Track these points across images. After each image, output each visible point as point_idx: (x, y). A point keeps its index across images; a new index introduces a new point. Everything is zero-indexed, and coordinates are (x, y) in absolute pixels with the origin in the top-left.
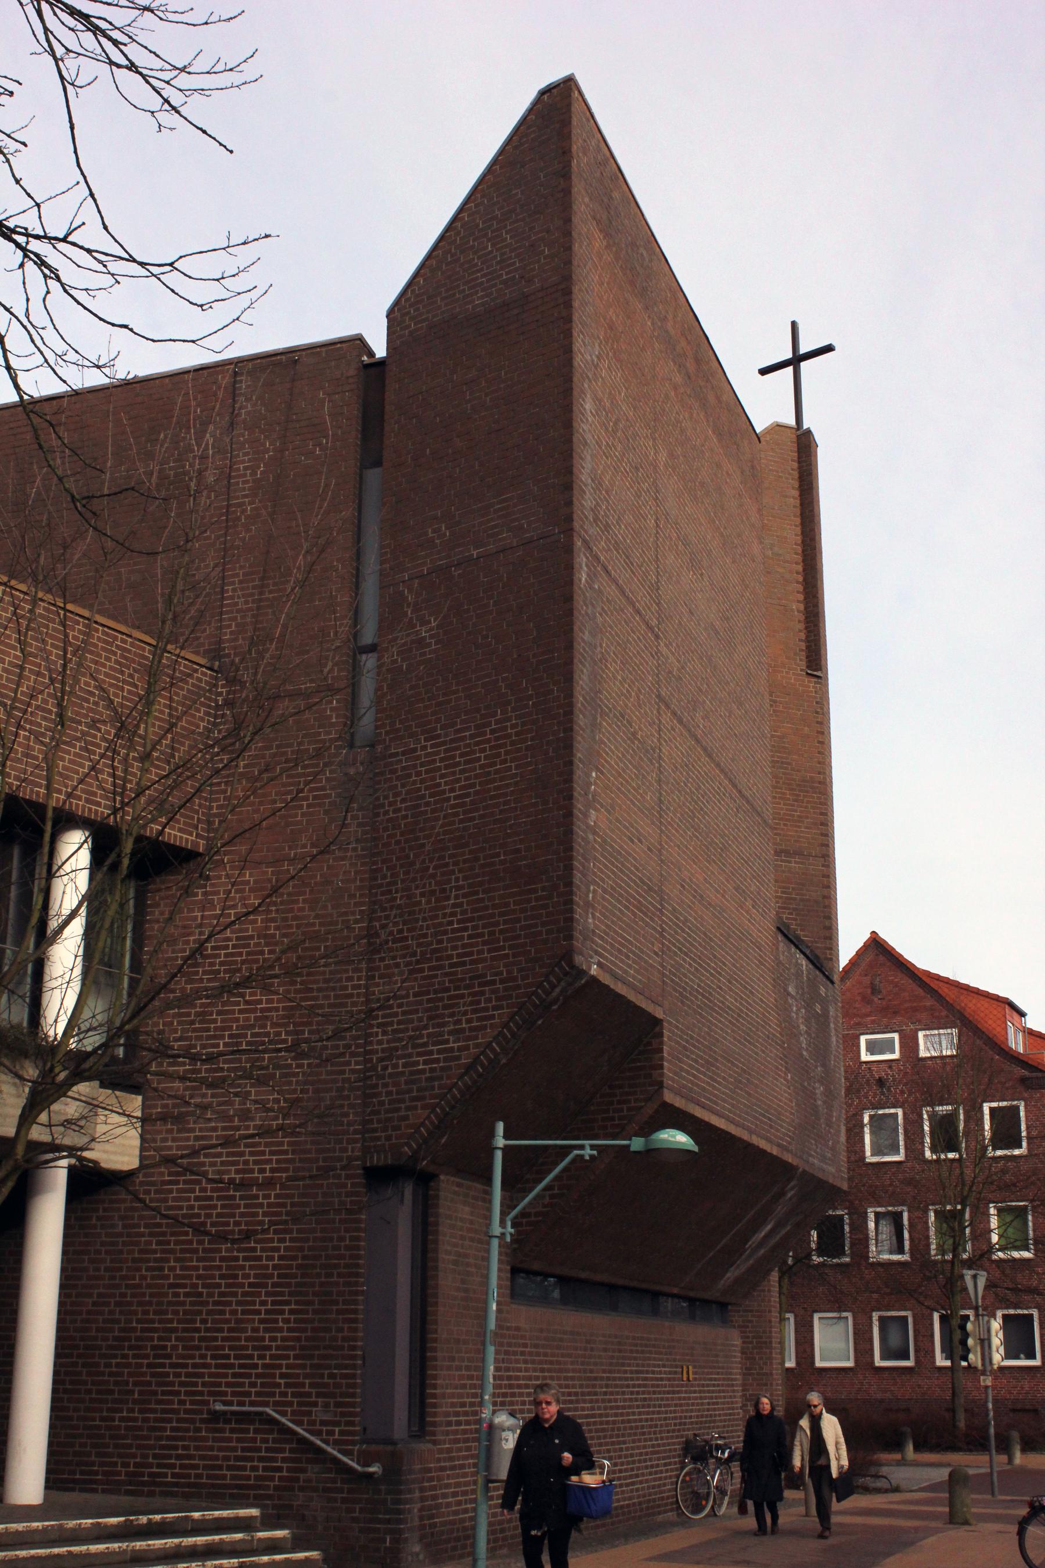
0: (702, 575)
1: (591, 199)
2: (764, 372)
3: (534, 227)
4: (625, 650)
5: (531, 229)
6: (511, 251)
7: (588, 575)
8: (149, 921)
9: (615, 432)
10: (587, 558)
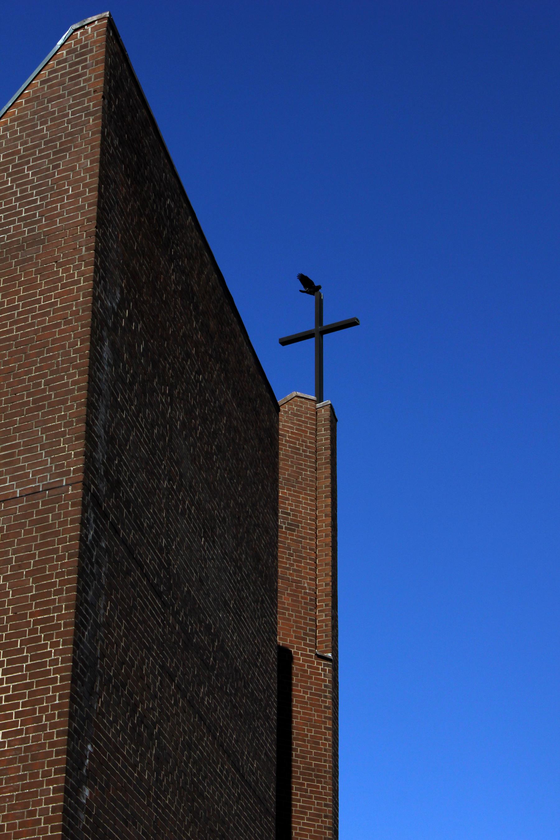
0: (214, 542)
1: (120, 143)
2: (285, 342)
3: (58, 166)
4: (240, 616)
5: (55, 167)
6: (32, 188)
7: (96, 532)
8: (327, 463)
9: (132, 384)
10: (95, 513)
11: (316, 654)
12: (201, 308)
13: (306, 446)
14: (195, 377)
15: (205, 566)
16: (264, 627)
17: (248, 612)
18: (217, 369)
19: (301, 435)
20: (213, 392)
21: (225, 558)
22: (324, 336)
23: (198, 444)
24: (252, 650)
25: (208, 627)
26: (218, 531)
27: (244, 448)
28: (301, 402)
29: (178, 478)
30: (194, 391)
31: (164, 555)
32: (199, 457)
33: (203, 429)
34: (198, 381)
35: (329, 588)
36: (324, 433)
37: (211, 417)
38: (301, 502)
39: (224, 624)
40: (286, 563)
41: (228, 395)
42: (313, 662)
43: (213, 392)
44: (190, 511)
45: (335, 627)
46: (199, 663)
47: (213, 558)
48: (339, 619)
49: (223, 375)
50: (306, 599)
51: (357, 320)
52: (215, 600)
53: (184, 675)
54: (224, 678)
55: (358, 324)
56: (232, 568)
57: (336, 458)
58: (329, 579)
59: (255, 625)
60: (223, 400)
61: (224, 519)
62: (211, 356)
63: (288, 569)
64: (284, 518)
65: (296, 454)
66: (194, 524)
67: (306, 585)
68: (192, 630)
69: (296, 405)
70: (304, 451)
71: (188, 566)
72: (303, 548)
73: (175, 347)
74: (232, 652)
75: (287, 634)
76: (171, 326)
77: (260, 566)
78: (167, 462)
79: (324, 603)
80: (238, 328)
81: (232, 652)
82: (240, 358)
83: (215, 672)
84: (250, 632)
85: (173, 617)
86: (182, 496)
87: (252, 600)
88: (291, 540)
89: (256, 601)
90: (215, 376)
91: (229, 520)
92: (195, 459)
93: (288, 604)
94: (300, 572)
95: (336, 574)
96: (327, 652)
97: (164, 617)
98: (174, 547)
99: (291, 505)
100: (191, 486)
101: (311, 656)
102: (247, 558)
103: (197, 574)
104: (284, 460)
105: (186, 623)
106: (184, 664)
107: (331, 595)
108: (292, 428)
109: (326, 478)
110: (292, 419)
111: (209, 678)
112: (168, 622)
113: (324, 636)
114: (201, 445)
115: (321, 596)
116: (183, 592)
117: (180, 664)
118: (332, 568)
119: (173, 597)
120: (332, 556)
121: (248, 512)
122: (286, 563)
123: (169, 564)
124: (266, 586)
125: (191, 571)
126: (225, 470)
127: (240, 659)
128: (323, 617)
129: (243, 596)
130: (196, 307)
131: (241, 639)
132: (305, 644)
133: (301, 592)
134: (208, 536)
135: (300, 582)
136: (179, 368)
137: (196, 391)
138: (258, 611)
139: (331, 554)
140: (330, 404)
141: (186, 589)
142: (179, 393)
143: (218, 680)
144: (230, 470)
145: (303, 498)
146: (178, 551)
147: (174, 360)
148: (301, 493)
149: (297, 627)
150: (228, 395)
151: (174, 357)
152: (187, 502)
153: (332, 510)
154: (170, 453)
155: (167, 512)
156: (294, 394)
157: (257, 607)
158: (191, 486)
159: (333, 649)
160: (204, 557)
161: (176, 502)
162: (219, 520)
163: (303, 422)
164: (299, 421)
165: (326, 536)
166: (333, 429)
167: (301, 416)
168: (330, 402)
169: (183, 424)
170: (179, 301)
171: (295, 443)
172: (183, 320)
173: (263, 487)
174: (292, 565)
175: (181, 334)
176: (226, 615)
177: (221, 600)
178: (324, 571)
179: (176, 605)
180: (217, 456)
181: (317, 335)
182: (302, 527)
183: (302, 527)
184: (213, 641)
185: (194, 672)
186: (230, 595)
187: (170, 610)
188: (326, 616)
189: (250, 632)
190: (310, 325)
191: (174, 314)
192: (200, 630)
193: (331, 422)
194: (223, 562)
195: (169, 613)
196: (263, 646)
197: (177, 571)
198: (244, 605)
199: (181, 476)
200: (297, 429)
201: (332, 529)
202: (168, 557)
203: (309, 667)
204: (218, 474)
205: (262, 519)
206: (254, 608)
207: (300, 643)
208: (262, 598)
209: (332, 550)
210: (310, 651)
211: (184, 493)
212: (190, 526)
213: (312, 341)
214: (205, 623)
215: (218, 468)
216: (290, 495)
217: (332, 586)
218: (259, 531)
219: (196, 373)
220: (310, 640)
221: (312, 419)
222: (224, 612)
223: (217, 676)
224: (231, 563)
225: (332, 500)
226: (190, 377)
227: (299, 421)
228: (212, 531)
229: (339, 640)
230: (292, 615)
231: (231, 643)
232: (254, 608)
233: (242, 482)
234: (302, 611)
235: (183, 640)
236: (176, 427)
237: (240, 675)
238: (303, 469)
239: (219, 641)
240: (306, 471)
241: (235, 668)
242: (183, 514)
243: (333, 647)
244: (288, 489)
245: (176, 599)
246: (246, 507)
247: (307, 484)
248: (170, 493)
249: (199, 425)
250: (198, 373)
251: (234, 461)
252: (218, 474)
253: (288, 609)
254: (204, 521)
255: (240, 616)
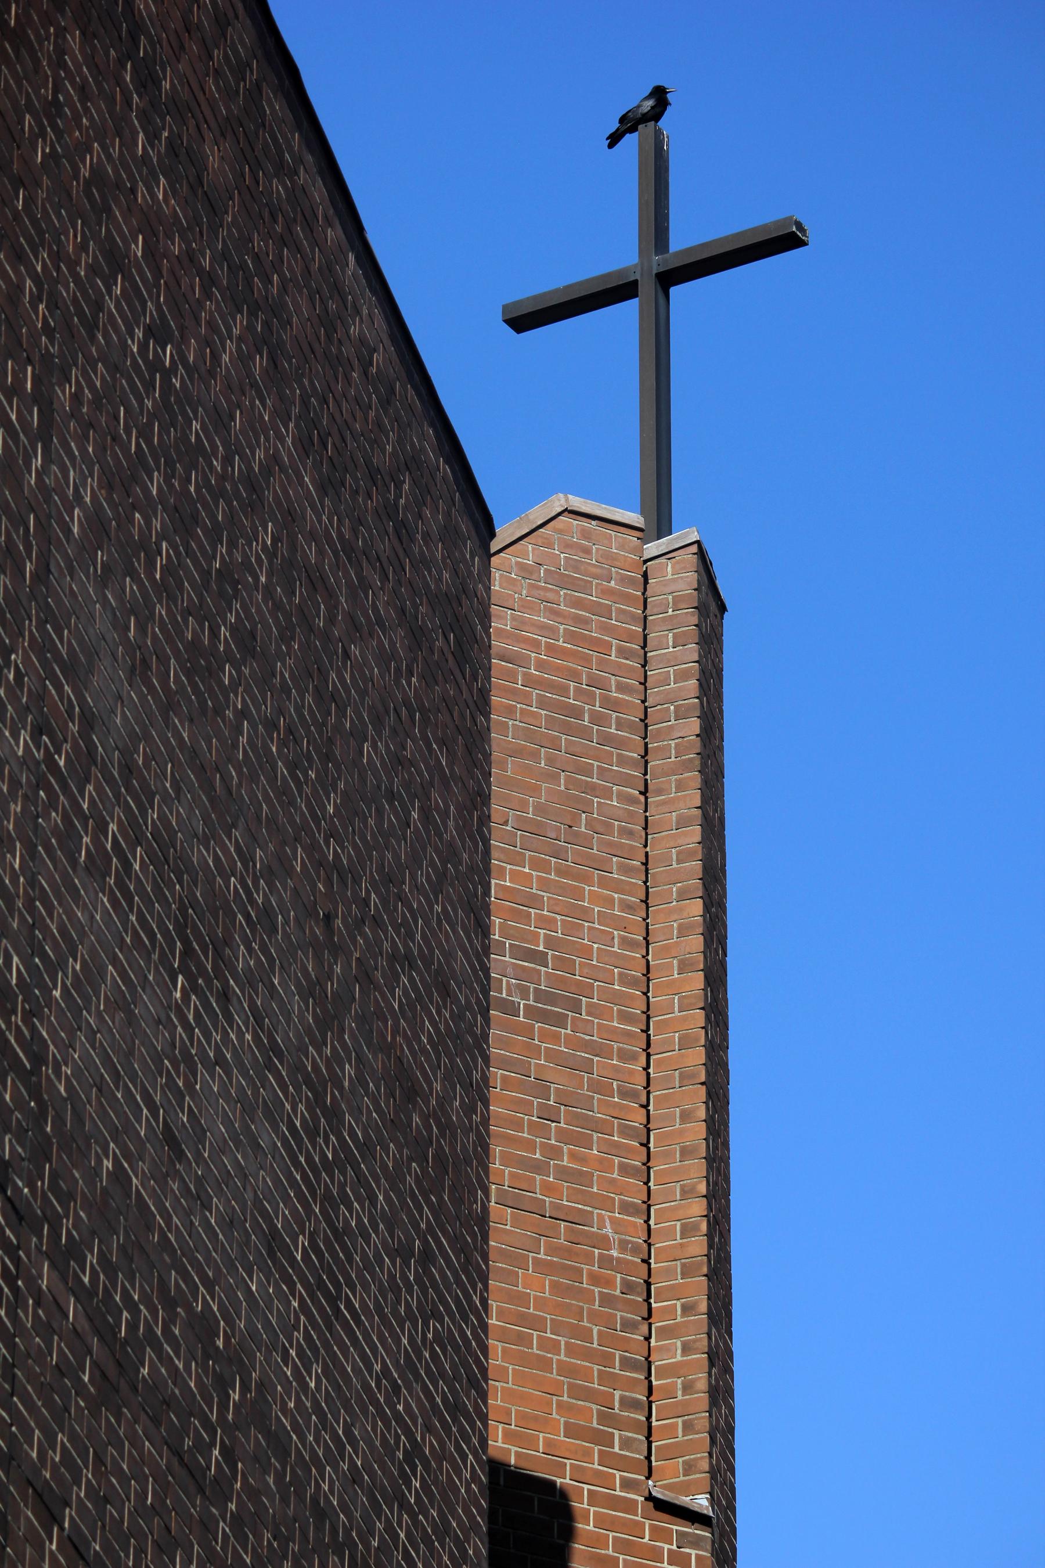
0: (225, 996)
2: (523, 321)
8: (686, 766)
11: (650, 1498)
12: (166, 85)
13: (606, 702)
14: (143, 347)
15: (190, 1086)
16: (433, 1354)
17: (366, 1287)
18: (236, 331)
19: (586, 660)
20: (220, 421)
21: (270, 1066)
22: (674, 291)
23: (161, 610)
24: (384, 1441)
25: (203, 1328)
26: (242, 960)
27: (346, 654)
28: (586, 534)
29: (74, 728)
30: (141, 403)
31: (18, 1019)
32: (163, 660)
33: (178, 554)
34: (156, 365)
35: (698, 1245)
36: (675, 656)
37: (213, 517)
38: (585, 914)
39: (267, 1324)
40: (531, 1146)
41: (281, 439)
42: (637, 1529)
43: (220, 421)
44: (127, 865)
45: (721, 1394)
46: (163, 1463)
47: (221, 1060)
48: (739, 1366)
49: (259, 363)
50: (609, 1283)
51: (799, 226)
52: (230, 1223)
53: (102, 1501)
54: (267, 1535)
55: (803, 243)
56: (301, 1107)
57: (721, 748)
58: (698, 1208)
59: (398, 1342)
60: (260, 454)
61: (267, 912)
62: (209, 280)
63: (539, 1168)
64: (522, 974)
65: (567, 729)
66: (141, 918)
67: (608, 1230)
68: (133, 1326)
69: (567, 546)
70: (597, 719)
71: (116, 1076)
72: (598, 1087)
73: (59, 216)
74: (302, 1438)
75: (536, 1418)
76: (43, 134)
77: (416, 1119)
78: (26, 659)
79: (680, 1298)
80: (319, 192)
81: (302, 1438)
82: (332, 306)
83: (232, 1506)
84: (377, 1367)
85: (53, 1265)
86: (92, 801)
87: (384, 1243)
88: (550, 1055)
89: (403, 1253)
90: (226, 358)
91: (286, 922)
92: (145, 663)
93: (540, 1303)
94: (584, 1178)
95: (727, 1193)
96: (686, 1488)
97: (17, 1262)
98: (57, 993)
99: (546, 923)
100: (128, 769)
101: (629, 1506)
102: (360, 1080)
103: (153, 1110)
104: (516, 752)
105: (108, 1295)
106: (99, 1460)
107: (705, 1270)
108: (551, 632)
109: (683, 823)
110: (550, 596)
111: (207, 1526)
112: (32, 1282)
113: (683, 1431)
114: (169, 611)
115: (669, 1273)
116: (97, 1171)
117: (84, 1454)
118: (710, 1167)
119: (54, 1187)
120: (709, 1121)
121: (366, 902)
122: (531, 1146)
123: (39, 1059)
124: (440, 1199)
125: (129, 1095)
126: (271, 725)
127: (336, 1468)
128: (679, 1354)
129: (346, 1222)
130: (148, 81)
131: (338, 1388)
132: (606, 1459)
133: (589, 1258)
134: (202, 971)
135: (584, 1219)
136: (75, 300)
137: (149, 403)
138: (410, 1292)
139: (702, 1114)
140: (698, 542)
141: (108, 1164)
142: (77, 398)
143: (243, 1541)
144: (290, 731)
145: (594, 898)
146: (77, 1012)
147: (58, 269)
148: (587, 879)
149: (576, 1392)
150: (282, 440)
151: (57, 257)
152: (113, 827)
153: (707, 944)
154: (41, 625)
155: (30, 851)
156: (558, 502)
157: (405, 1278)
158: (128, 769)
159: (713, 1478)
160: (185, 1052)
161: (66, 818)
162: (247, 917)
163: (596, 609)
164: (578, 604)
165: (685, 1043)
166: (710, 641)
167: (586, 587)
168: (694, 537)
169: (96, 522)
170: (74, 41)
171: (563, 691)
172: (91, 119)
173: (426, 815)
174: (555, 1153)
175: (85, 172)
176: (277, 1287)
177: (256, 1224)
178: (681, 1177)
179: (67, 1224)
180: (236, 665)
181: (648, 287)
182: (592, 1010)
183: (592, 1010)
184: (223, 1385)
185: (142, 1495)
186: (294, 1211)
187: (40, 1237)
188: (686, 1349)
189: (377, 1367)
190: (621, 252)
191: (56, 90)
192: (166, 1330)
193: (701, 609)
194: (264, 1081)
195: (38, 1249)
196: (428, 1428)
197: (69, 1087)
198: (350, 1259)
199: (88, 722)
200: (570, 637)
201: (708, 1018)
202: (33, 1029)
203: (622, 1546)
204: (243, 740)
205: (424, 936)
206: (392, 1277)
207: (587, 1454)
208: (425, 1242)
209: (709, 1094)
210: (627, 1484)
211: (99, 789)
212: (125, 922)
213: (629, 310)
214: (189, 1309)
215: (243, 714)
216: (544, 885)
217: (710, 1235)
218: (411, 980)
219: (149, 331)
220: (626, 1443)
221: (627, 598)
222: (268, 1276)
223: (237, 1522)
224: (298, 1089)
225: (707, 907)
226: (124, 346)
227: (578, 604)
228: (218, 954)
229: (737, 1446)
230: (555, 1347)
231: (298, 1401)
232: (392, 1277)
233: (342, 785)
234: (595, 1329)
235: (95, 1364)
236: (68, 532)
237: (334, 1531)
238: (592, 789)
239: (245, 1388)
240: (607, 794)
241: (315, 1500)
242: (97, 866)
243: (713, 1472)
244: (535, 865)
245: (66, 1197)
246: (357, 881)
247: (610, 844)
248: (41, 783)
249: (163, 536)
250: (158, 333)
251: (309, 699)
252: (243, 740)
253: (538, 1324)
254: (183, 909)
255: (333, 1301)
